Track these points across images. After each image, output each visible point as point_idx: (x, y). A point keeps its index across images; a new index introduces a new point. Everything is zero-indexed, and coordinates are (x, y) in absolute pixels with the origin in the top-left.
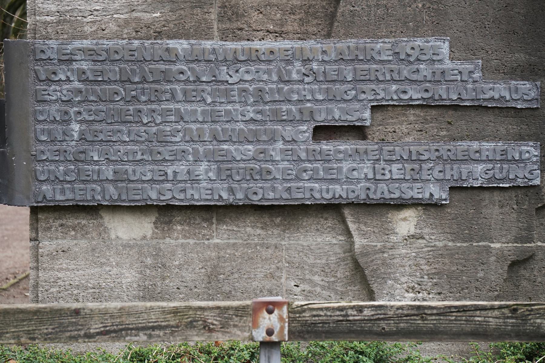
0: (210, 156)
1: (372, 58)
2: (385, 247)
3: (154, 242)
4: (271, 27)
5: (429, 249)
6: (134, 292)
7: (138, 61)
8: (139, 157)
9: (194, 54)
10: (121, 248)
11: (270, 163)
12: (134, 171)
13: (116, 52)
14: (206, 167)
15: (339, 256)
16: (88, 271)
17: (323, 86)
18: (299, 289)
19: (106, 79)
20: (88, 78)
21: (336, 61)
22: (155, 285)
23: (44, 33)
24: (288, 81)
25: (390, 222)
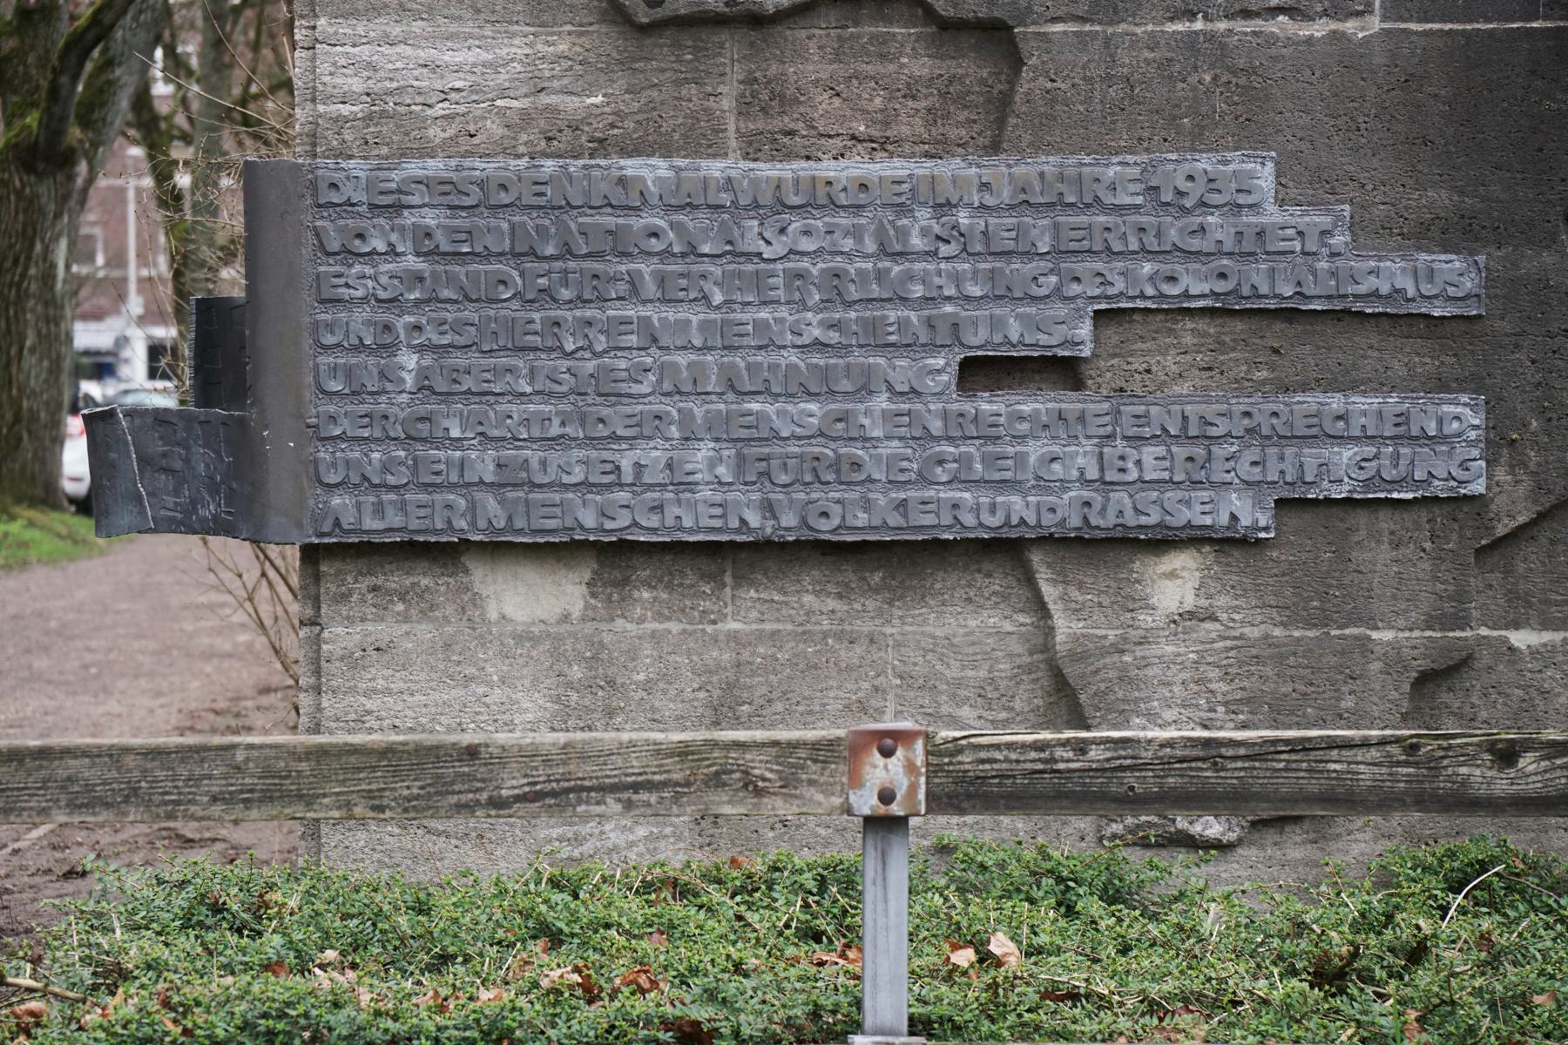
0: (719, 429)
1: (1097, 199)
2: (1125, 639)
3: (589, 628)
4: (862, 128)
5: (1229, 643)
7: (553, 208)
8: (555, 430)
9: (685, 189)
11: (859, 445)
12: (544, 463)
14: (711, 453)
15: (1018, 661)
16: (435, 696)
19: (479, 249)
21: (1012, 207)
25: (1138, 582)
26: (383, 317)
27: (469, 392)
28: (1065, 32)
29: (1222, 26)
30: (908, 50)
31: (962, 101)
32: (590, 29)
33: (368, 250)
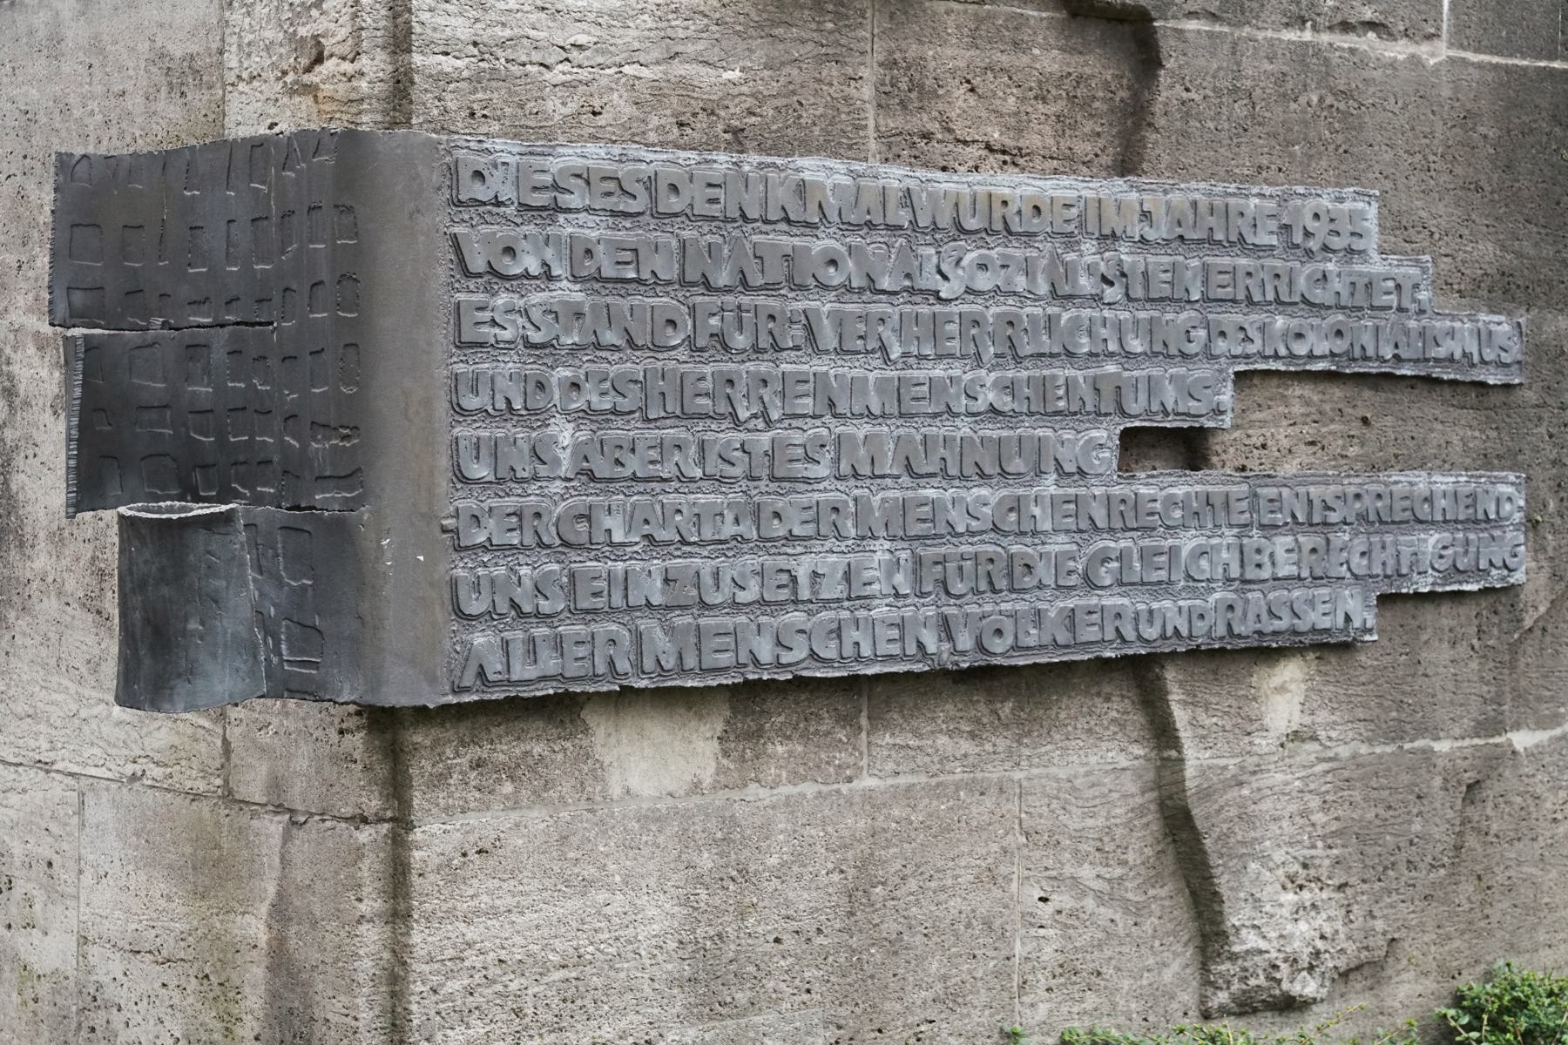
4: (996, 135)
6: (670, 967)
7: (726, 220)
8: (729, 530)
10: (637, 826)
11: (1028, 540)
12: (716, 575)
13: (674, 188)
17: (1142, 315)
18: (1048, 909)
19: (646, 275)
23: (436, 112)
24: (1071, 297)
25: (1255, 699)
26: (532, 369)
27: (634, 478)
28: (1199, 32)
29: (1325, 38)
31: (1086, 104)
33: (518, 271)
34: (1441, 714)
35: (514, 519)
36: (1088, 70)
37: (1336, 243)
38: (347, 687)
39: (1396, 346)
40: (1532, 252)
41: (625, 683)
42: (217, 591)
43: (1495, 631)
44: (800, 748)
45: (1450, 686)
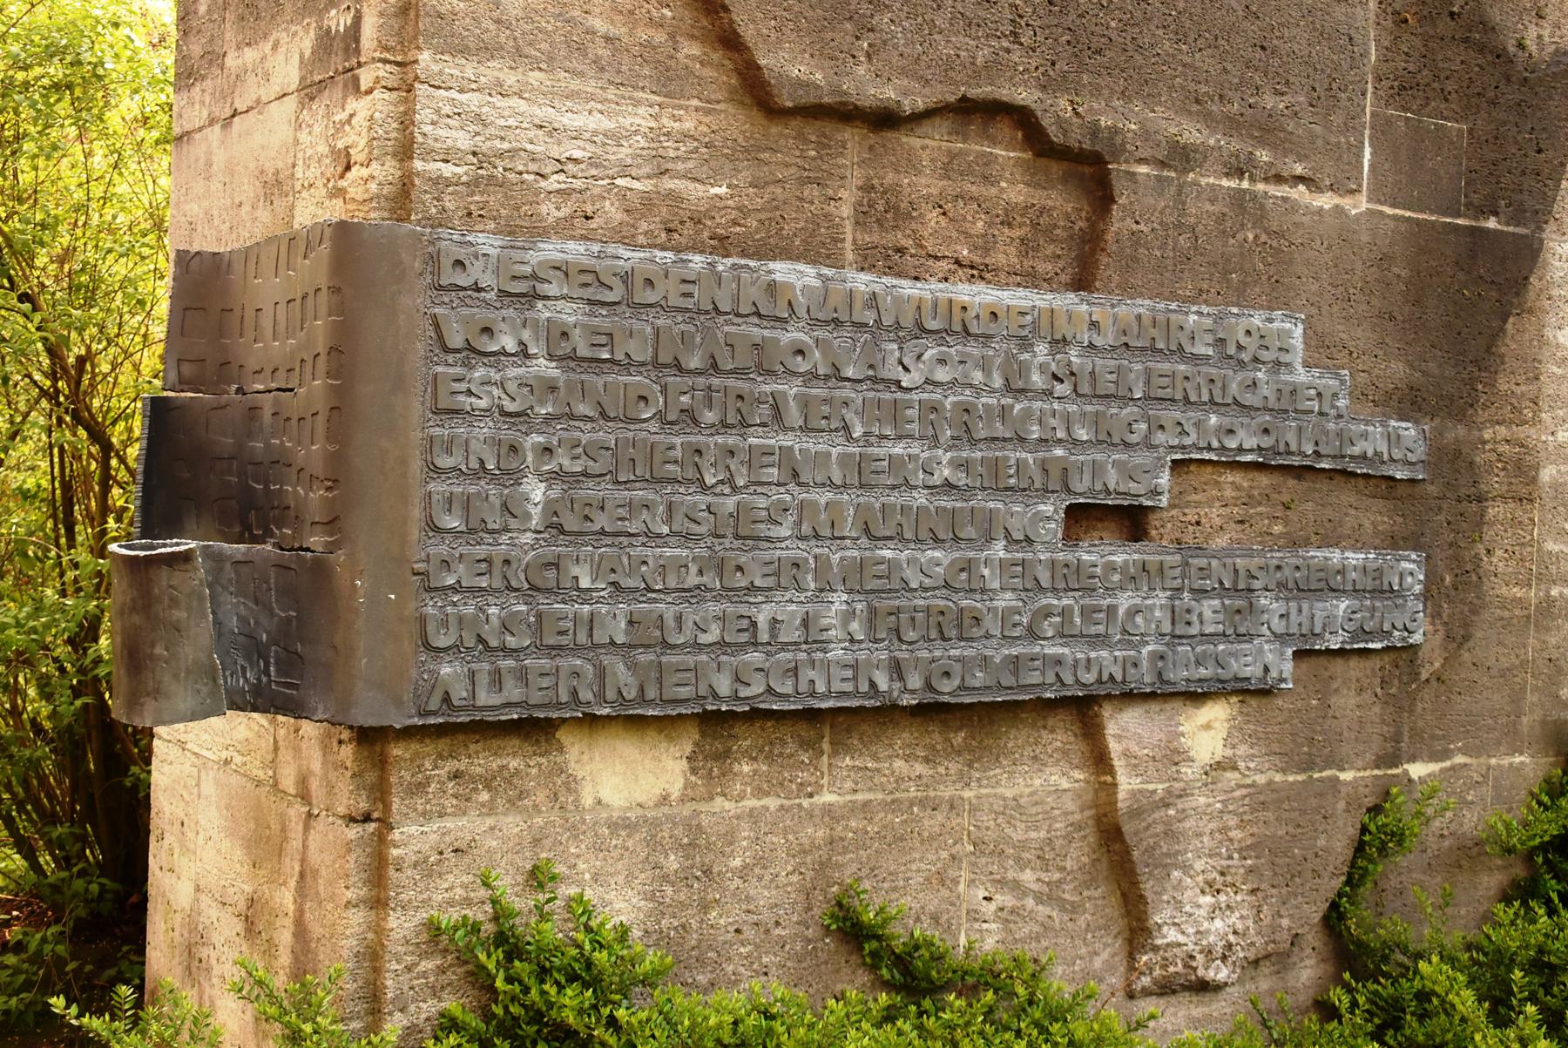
0: (856, 577)
1: (1181, 348)
2: (1168, 791)
3: (687, 810)
7: (699, 312)
8: (692, 580)
9: (831, 303)
11: (978, 597)
12: (679, 619)
14: (844, 607)
15: (1071, 819)
17: (1089, 408)
18: (992, 906)
19: (619, 356)
20: (574, 350)
21: (1114, 348)
22: (683, 927)
23: (434, 210)
24: (1022, 391)
26: (508, 435)
27: (603, 532)
29: (1261, 187)
30: (1007, 175)
31: (1048, 232)
32: (718, 107)
34: (1346, 749)
35: (484, 565)
36: (1050, 203)
37: (1265, 355)
38: (321, 707)
39: (1317, 444)
40: (1437, 372)
41: (588, 710)
42: (178, 621)
43: (1396, 682)
44: (764, 768)
45: (1356, 727)
